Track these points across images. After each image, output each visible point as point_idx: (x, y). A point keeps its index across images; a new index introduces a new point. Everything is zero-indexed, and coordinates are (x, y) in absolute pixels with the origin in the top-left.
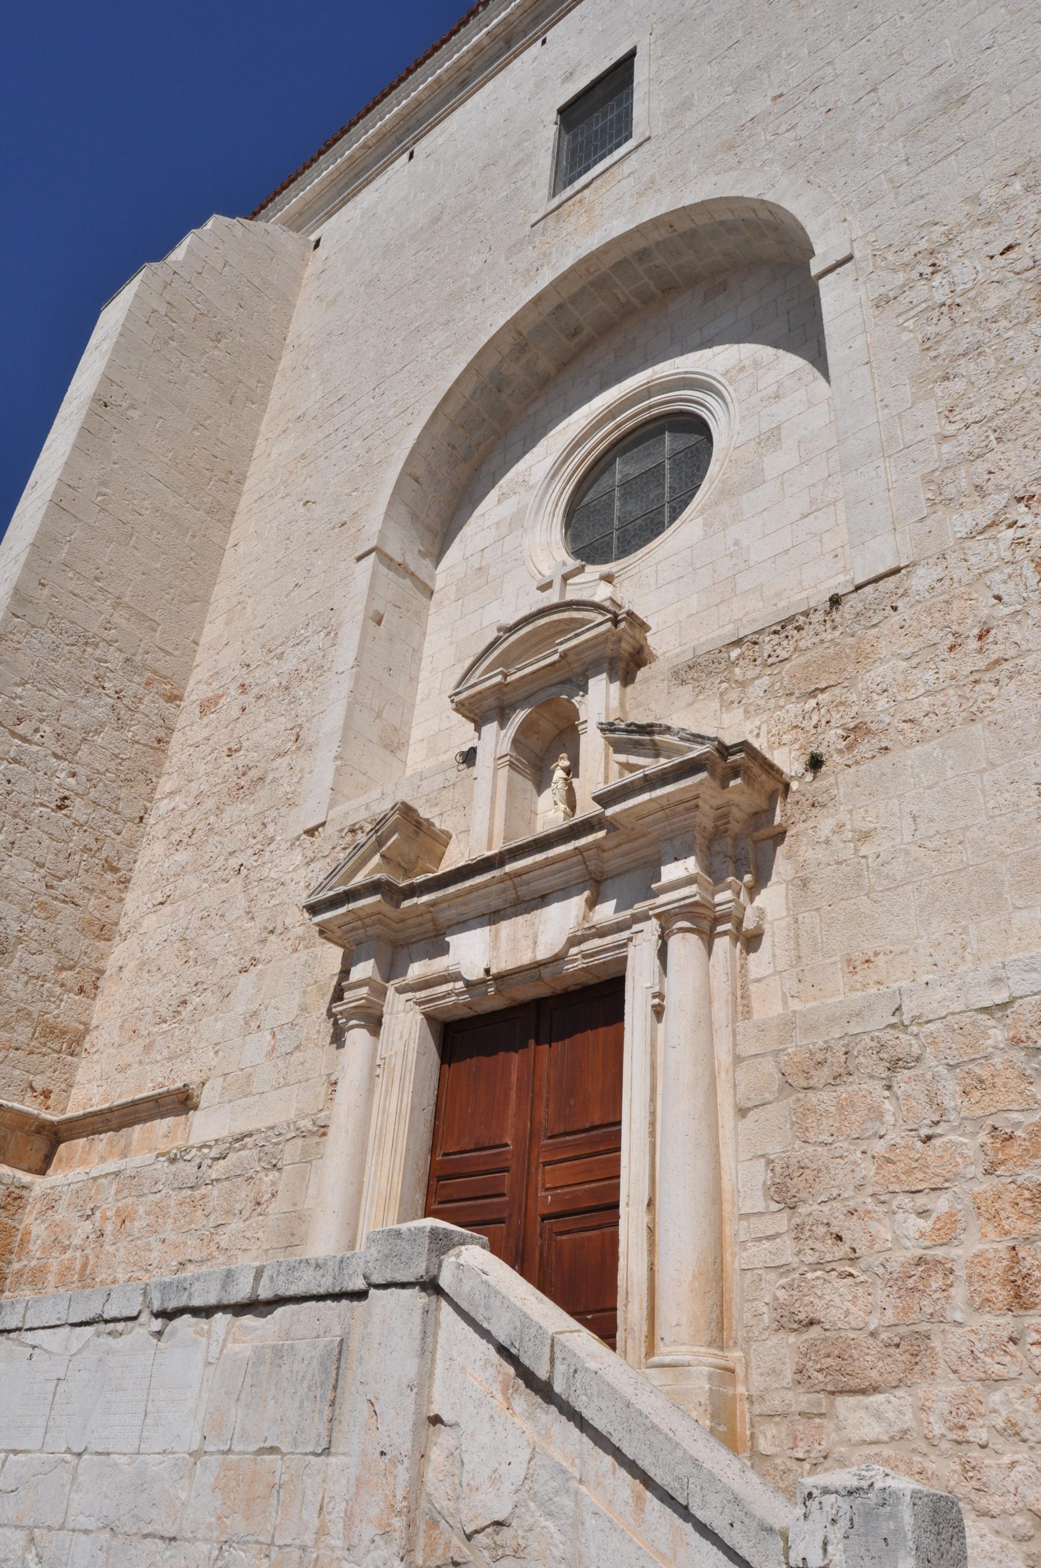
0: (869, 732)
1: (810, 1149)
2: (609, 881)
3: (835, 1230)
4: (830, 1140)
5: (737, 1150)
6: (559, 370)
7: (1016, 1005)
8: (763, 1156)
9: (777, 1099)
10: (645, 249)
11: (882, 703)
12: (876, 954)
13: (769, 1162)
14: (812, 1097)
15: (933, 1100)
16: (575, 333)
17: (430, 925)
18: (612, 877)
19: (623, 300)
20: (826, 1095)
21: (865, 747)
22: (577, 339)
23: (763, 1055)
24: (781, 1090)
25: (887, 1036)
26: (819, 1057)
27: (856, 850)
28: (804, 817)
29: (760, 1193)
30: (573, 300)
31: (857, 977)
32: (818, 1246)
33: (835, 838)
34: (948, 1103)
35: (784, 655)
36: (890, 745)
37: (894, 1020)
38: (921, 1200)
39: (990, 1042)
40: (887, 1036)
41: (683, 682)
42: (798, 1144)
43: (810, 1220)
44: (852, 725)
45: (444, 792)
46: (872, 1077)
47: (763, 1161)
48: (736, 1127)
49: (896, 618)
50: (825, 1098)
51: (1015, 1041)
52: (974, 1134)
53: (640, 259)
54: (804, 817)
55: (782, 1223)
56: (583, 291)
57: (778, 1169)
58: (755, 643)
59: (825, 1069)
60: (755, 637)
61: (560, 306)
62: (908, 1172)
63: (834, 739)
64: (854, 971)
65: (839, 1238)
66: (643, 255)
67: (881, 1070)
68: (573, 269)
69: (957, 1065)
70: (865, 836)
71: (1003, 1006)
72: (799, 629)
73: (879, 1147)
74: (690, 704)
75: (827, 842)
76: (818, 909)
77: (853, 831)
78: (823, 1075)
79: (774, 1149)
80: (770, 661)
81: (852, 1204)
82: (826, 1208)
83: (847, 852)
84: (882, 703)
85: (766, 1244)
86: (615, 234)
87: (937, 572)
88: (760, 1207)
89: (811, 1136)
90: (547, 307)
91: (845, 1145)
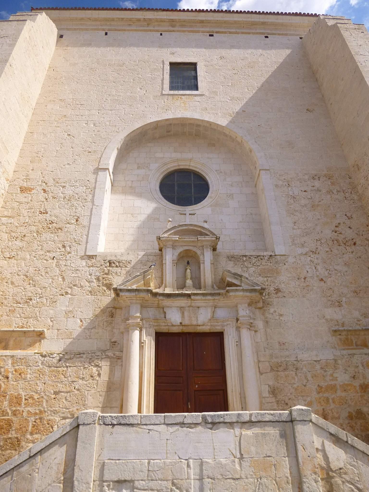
0: (280, 291)
1: (279, 384)
2: (218, 308)
3: (286, 402)
4: (284, 383)
5: (261, 382)
6: (159, 138)
7: (321, 361)
8: (268, 384)
9: (270, 372)
10: (200, 125)
11: (283, 285)
12: (285, 343)
13: (269, 386)
14: (279, 373)
15: (306, 377)
16: (169, 132)
17: (156, 305)
18: (218, 307)
19: (185, 131)
20: (282, 373)
21: (280, 294)
22: (168, 133)
23: (266, 361)
24: (271, 370)
25: (295, 362)
26: (280, 364)
27: (279, 318)
28: (266, 306)
29: (267, 393)
30: (174, 125)
31: (281, 347)
32: (283, 405)
33: (274, 313)
34: (309, 379)
35: (258, 264)
36: (286, 296)
37: (296, 359)
38: (305, 398)
39: (317, 368)
40: (295, 362)
41: (230, 260)
42: (276, 383)
43: (281, 400)
44: (276, 288)
45: (148, 262)
46: (292, 371)
47: (268, 386)
48: (260, 377)
49: (285, 266)
50: (282, 374)
51: (322, 368)
52: (314, 386)
53: (197, 126)
54: (266, 306)
55: (274, 400)
56: (178, 124)
57: (272, 387)
58: (250, 258)
59: (282, 367)
60: (250, 257)
61: (171, 124)
62: (302, 392)
63: (272, 290)
64: (281, 346)
65: (287, 404)
66: (198, 126)
67: (294, 369)
68: (180, 118)
69: (310, 371)
70: (281, 315)
71: (319, 361)
72: (261, 259)
73: (295, 386)
74: (232, 267)
75: (272, 314)
76: (271, 329)
77: (278, 313)
78: (281, 369)
79: (271, 383)
80: (255, 264)
81: (290, 397)
82: (284, 397)
83: (277, 318)
84: (283, 285)
85: (270, 404)
86: (195, 117)
87: (294, 260)
88: (268, 396)
89: (279, 381)
90: (168, 123)
91: (287, 384)
